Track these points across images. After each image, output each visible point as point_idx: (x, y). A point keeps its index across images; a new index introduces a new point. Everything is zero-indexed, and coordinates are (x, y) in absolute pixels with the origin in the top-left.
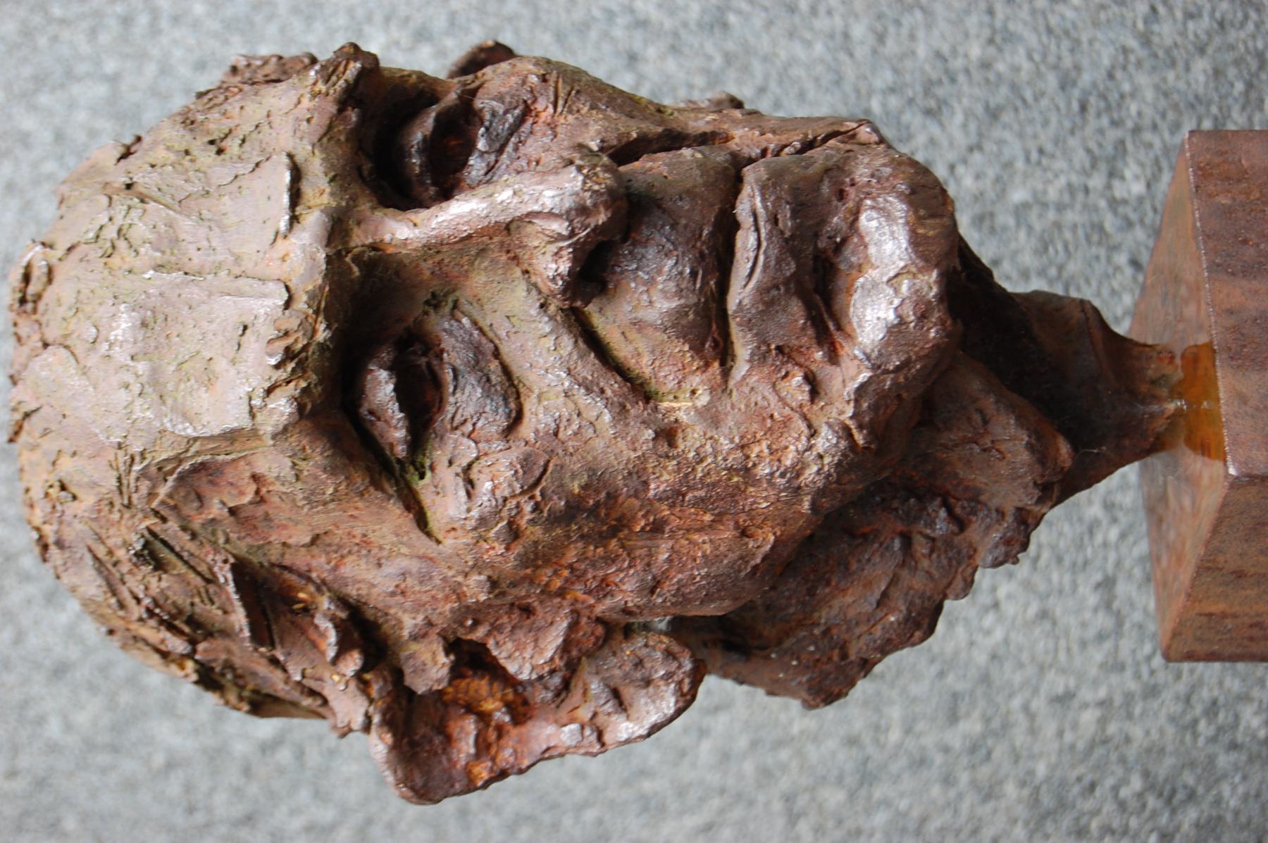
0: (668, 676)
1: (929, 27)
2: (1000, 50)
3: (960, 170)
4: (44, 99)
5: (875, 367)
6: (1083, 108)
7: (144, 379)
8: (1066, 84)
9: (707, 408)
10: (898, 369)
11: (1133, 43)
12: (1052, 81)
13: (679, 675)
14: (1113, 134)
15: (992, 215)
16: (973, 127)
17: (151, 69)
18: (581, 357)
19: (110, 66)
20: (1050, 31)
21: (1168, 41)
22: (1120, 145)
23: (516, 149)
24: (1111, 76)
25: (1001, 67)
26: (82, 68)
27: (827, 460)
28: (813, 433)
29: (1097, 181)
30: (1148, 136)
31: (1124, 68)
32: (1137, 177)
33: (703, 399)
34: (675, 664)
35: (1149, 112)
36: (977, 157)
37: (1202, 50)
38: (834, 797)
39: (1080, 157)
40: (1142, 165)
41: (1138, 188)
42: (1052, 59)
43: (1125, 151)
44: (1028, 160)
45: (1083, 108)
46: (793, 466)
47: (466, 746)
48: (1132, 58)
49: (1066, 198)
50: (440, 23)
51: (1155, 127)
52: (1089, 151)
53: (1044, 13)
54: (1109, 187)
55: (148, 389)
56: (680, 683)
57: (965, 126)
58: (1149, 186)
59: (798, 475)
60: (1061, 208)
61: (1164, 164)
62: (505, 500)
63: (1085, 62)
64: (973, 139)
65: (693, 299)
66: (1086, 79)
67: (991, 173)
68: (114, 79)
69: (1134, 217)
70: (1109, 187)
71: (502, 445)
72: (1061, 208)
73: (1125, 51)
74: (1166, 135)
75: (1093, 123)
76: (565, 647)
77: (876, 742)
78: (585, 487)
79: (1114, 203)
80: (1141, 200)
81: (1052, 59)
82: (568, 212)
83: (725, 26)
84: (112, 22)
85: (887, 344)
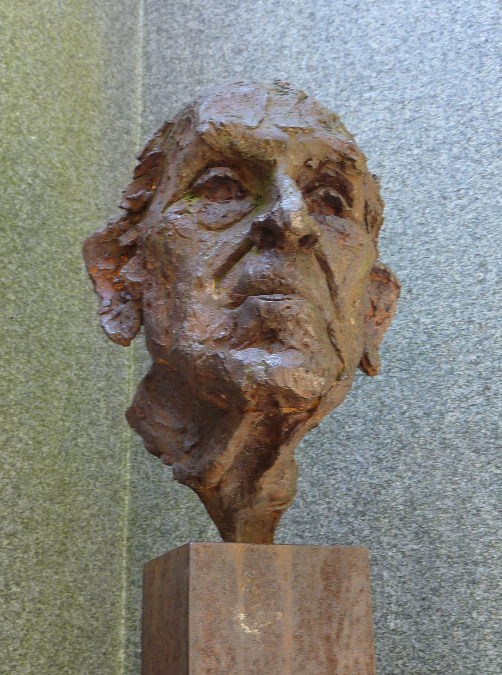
0: (122, 329)
1: (452, 531)
2: (445, 561)
3: (395, 550)
4: (396, 212)
5: (224, 359)
6: (424, 599)
7: (223, 96)
8: (435, 591)
9: (212, 299)
10: (225, 369)
11: (453, 619)
12: (435, 585)
13: (122, 333)
14: (413, 613)
15: (377, 565)
16: (412, 553)
17: (410, 245)
18: (232, 247)
19: (409, 231)
20: (455, 582)
21: (455, 634)
22: (409, 617)
23: (327, 230)
24: (438, 610)
25: (438, 563)
26: (407, 222)
27: (189, 349)
28: (201, 343)
29: (394, 608)
30: (414, 629)
31: (442, 616)
32: (396, 625)
33: (215, 297)
34: (127, 331)
35: (424, 628)
36: (400, 556)
37: (452, 650)
38: (157, 523)
39: (403, 599)
40: (402, 626)
41: (392, 626)
42: (443, 584)
43: (407, 619)
44: (400, 577)
45: (424, 599)
46: (186, 335)
47: (103, 266)
48: (446, 619)
49: (386, 595)
50: (435, 342)
51: (418, 631)
52: (406, 603)
53: (461, 579)
54: (392, 613)
55: (219, 97)
56: (120, 335)
57: (413, 550)
58: (394, 630)
59: (183, 339)
60: (382, 593)
61: (403, 636)
62: (173, 223)
63: (442, 598)
64: (407, 553)
65: (253, 279)
66: (435, 599)
67: (394, 563)
68: (405, 234)
69: (380, 625)
70: (392, 613)
71: (196, 221)
72: (382, 593)
73: (449, 616)
74: (415, 637)
75: (417, 604)
76: (133, 284)
77: (176, 537)
78: (179, 255)
79: (385, 616)
80: (387, 627)
81: (443, 584)
82: (281, 208)
83: (445, 448)
84: (425, 229)
85: (235, 362)
